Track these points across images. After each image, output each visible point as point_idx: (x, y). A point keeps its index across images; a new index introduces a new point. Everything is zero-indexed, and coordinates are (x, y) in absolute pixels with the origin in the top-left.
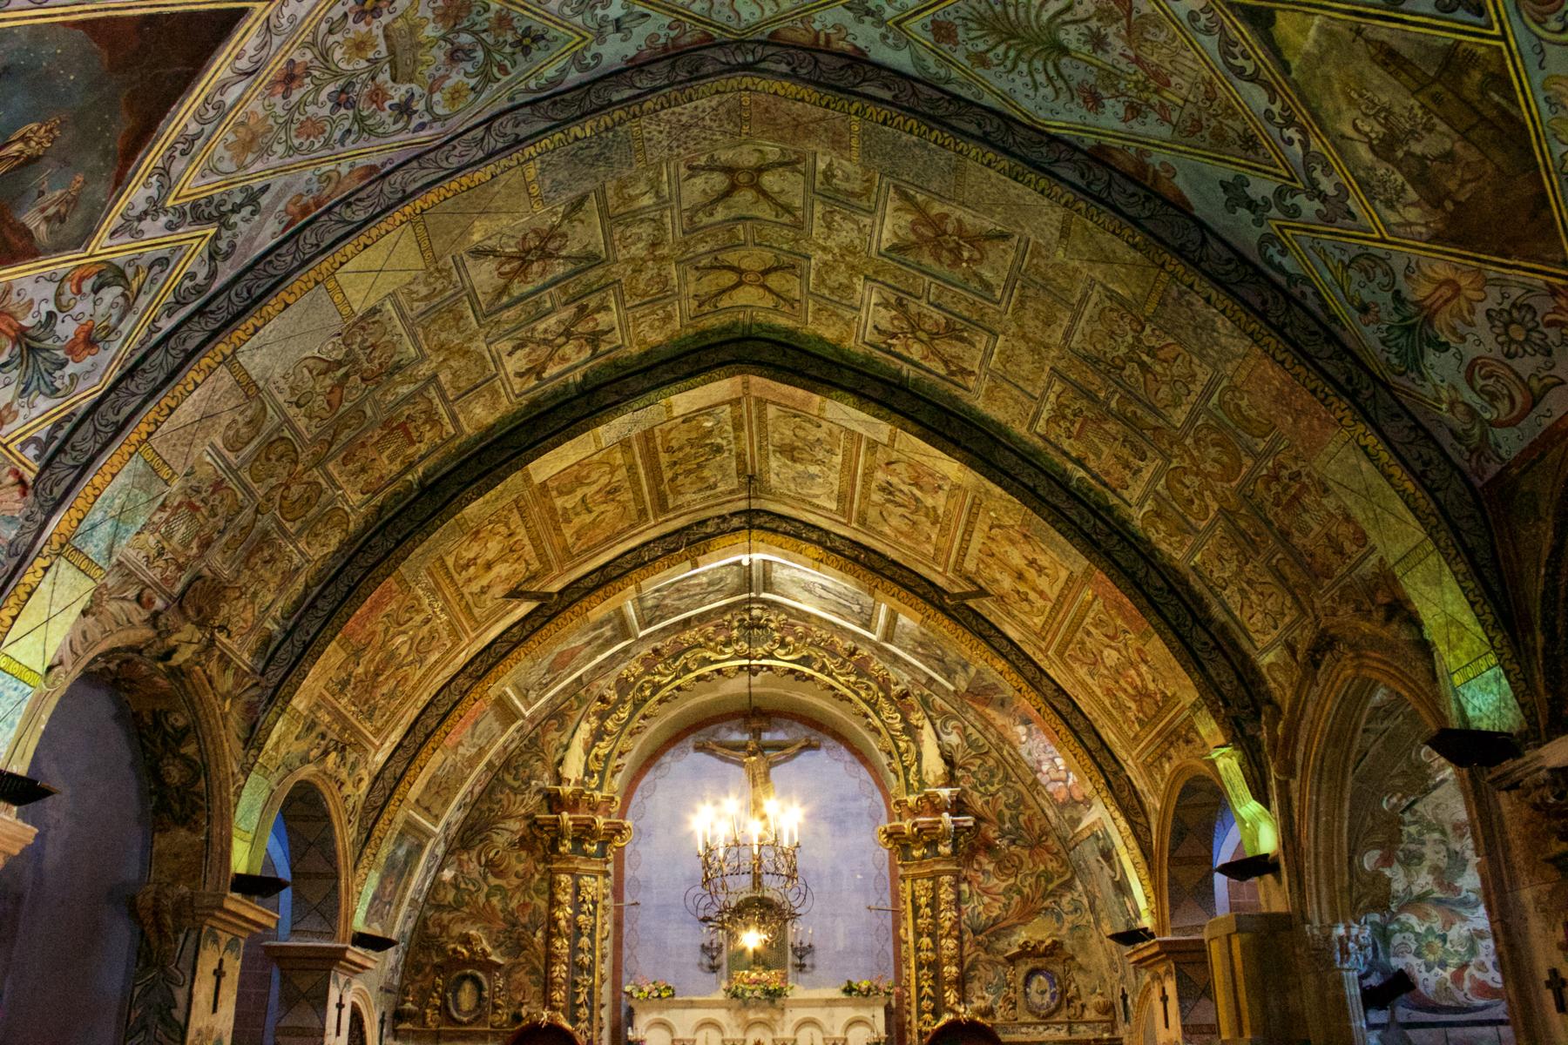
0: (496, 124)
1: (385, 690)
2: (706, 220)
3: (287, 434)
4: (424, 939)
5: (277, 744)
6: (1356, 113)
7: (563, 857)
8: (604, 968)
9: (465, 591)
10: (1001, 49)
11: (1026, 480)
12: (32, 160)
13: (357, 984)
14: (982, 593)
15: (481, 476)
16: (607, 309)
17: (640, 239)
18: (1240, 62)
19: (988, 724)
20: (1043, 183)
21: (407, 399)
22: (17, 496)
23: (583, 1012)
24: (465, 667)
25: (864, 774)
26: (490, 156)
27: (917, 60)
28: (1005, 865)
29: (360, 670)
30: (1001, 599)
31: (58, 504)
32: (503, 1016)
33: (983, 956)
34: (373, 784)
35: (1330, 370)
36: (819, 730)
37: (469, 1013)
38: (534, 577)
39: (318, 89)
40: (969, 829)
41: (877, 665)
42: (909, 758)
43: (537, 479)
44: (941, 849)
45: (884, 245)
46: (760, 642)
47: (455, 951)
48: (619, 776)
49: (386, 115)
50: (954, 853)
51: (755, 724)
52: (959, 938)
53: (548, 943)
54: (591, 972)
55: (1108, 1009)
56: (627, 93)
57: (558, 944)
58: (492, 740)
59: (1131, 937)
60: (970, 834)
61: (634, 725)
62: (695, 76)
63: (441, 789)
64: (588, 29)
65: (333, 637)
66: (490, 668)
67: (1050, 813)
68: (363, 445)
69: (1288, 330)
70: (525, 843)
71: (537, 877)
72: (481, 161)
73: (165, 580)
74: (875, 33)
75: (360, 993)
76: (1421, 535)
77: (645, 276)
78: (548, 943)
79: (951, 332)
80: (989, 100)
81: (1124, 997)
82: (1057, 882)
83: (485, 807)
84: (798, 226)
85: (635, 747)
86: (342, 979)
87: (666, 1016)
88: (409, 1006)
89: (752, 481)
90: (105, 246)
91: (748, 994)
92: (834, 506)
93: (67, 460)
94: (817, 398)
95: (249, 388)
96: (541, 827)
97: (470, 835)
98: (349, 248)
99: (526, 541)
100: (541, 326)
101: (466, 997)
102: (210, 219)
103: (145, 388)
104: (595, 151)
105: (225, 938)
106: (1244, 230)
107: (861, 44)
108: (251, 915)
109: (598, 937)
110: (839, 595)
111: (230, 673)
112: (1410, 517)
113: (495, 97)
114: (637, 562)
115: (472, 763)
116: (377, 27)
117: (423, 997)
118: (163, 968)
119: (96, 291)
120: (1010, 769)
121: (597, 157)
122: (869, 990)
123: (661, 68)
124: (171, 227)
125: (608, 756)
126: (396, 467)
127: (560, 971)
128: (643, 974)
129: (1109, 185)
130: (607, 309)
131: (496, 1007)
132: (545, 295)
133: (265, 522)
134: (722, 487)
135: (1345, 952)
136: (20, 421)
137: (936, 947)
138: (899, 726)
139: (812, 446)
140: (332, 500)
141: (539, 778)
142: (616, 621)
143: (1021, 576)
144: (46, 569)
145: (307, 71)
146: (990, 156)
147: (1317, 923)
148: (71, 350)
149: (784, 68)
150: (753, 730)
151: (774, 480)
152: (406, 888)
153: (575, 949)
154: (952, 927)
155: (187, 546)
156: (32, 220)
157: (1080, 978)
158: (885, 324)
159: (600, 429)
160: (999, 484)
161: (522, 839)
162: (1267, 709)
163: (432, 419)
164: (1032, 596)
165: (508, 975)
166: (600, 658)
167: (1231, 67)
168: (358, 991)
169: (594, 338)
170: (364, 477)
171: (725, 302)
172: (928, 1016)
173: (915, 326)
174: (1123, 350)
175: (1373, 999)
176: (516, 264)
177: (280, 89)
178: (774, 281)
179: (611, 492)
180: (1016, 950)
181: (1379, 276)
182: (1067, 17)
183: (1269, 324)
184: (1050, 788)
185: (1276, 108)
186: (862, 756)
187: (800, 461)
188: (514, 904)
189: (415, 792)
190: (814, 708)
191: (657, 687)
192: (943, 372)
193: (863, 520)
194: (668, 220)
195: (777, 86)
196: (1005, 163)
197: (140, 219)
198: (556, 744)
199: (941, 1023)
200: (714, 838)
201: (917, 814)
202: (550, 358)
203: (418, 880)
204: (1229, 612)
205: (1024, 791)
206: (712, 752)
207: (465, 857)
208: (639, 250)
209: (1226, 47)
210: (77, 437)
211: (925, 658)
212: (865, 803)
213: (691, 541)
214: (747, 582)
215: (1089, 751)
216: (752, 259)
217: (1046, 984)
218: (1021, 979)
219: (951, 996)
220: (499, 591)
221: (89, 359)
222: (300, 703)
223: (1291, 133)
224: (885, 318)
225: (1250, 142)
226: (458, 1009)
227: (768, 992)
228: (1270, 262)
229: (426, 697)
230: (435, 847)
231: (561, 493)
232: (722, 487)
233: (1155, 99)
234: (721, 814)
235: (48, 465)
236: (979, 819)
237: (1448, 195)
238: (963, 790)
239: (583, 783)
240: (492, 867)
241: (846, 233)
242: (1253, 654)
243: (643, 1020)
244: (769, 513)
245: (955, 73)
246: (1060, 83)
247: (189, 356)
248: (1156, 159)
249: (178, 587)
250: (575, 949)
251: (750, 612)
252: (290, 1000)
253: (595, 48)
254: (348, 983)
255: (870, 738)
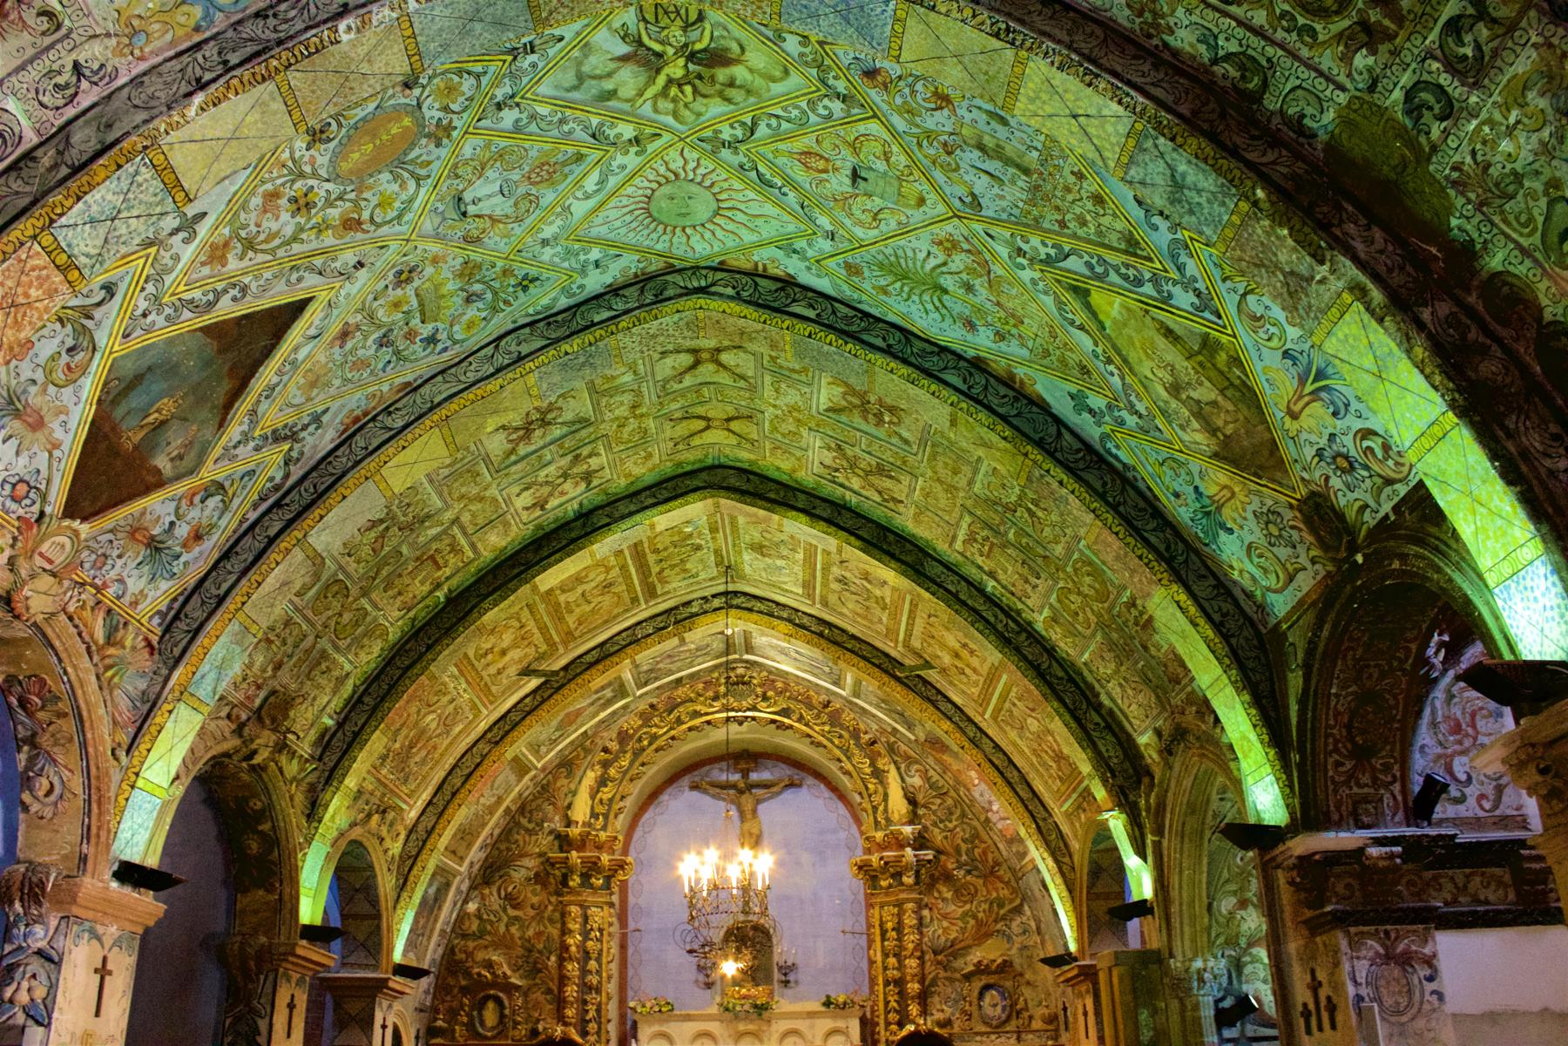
0: (503, 343)
1: (417, 759)
2: (676, 386)
3: (341, 577)
4: (451, 964)
5: (333, 817)
6: (1151, 364)
7: (572, 891)
8: (612, 987)
9: (484, 674)
10: (898, 285)
11: (950, 587)
12: (163, 423)
13: (397, 1006)
14: (928, 665)
15: (495, 591)
16: (598, 455)
17: (622, 404)
18: (1070, 316)
19: (946, 769)
20: (933, 387)
21: (436, 538)
22: (147, 656)
23: (592, 1027)
24: (485, 733)
25: (842, 809)
26: (498, 371)
27: (835, 285)
28: (962, 893)
29: (397, 745)
30: (944, 671)
31: (178, 661)
32: (522, 1031)
33: (942, 974)
34: (408, 837)
35: (1153, 540)
36: (801, 770)
37: (493, 1028)
38: (541, 657)
39: (366, 338)
40: (929, 861)
41: (848, 717)
42: (877, 799)
43: (543, 588)
44: (905, 879)
45: (822, 407)
46: (742, 696)
47: (479, 974)
48: (621, 817)
49: (418, 346)
50: (917, 883)
51: (743, 765)
52: (921, 958)
53: (561, 966)
54: (598, 991)
55: (1051, 1019)
56: (606, 314)
57: (570, 967)
58: (508, 791)
59: (1060, 960)
60: (929, 867)
61: (634, 771)
62: (660, 300)
63: (466, 835)
64: (573, 270)
65: (377, 727)
66: (507, 733)
67: (1001, 846)
68: (400, 575)
69: (1121, 509)
70: (540, 879)
71: (550, 908)
72: (492, 375)
73: (248, 698)
74: (803, 265)
75: (399, 1015)
76: (1219, 671)
77: (627, 429)
78: (561, 966)
79: (881, 470)
80: (891, 318)
81: (1065, 1009)
82: (1008, 907)
83: (503, 846)
84: (752, 389)
85: (636, 790)
86: (385, 1004)
87: (664, 1028)
88: (440, 1023)
89: (728, 570)
90: (210, 472)
91: (738, 1008)
92: (800, 591)
93: (182, 625)
94: (776, 517)
95: (317, 560)
96: (553, 865)
97: (491, 871)
98: (391, 451)
99: (535, 631)
100: (542, 473)
101: (490, 1015)
102: (286, 438)
103: (238, 568)
104: (582, 359)
105: (295, 976)
106: (1091, 430)
107: (791, 271)
108: (315, 958)
109: (604, 960)
110: (811, 659)
111: (295, 762)
112: (1211, 656)
113: (501, 323)
114: (631, 639)
115: (491, 811)
116: (409, 290)
117: (452, 1014)
118: (248, 1004)
119: (202, 502)
120: (965, 809)
121: (583, 365)
122: (845, 1003)
123: (632, 292)
124: (257, 449)
125: (611, 800)
126: (426, 588)
127: (571, 991)
128: (647, 987)
129: (986, 388)
130: (598, 455)
131: (516, 1023)
132: (546, 451)
133: (324, 643)
134: (703, 576)
135: (1201, 980)
136: (149, 599)
137: (901, 966)
138: (868, 770)
139: (777, 545)
140: (375, 619)
141: (551, 820)
142: (616, 686)
143: (957, 655)
144: (170, 712)
145: (358, 328)
146: (892, 365)
147: (1180, 958)
148: (184, 545)
149: (730, 291)
150: (742, 771)
151: (748, 570)
152: (436, 921)
153: (584, 972)
154: (915, 949)
155: (264, 671)
156: (162, 462)
157: (1027, 992)
158: (828, 462)
159: (595, 547)
160: (927, 590)
161: (537, 875)
162: (1146, 780)
163: (455, 549)
164: (967, 671)
165: (526, 995)
166: (602, 715)
167: (1066, 319)
168: (397, 1014)
169: (587, 477)
170: (400, 598)
171: (696, 441)
172: (894, 1027)
173: (853, 465)
174: (1014, 498)
175: (1224, 1018)
176: (521, 433)
177: (338, 343)
178: (734, 425)
179: (607, 586)
180: (971, 968)
181: (1183, 476)
182: (944, 269)
183: (1107, 503)
184: (1000, 826)
185: (1100, 350)
186: (842, 796)
187: (769, 556)
188: (530, 933)
189: (443, 842)
190: (793, 750)
191: (654, 737)
192: (878, 499)
193: (825, 603)
194: (644, 389)
195: (725, 306)
196: (905, 370)
197: (235, 447)
198: (565, 790)
199: (904, 1033)
200: (698, 881)
201: (885, 849)
202: (551, 494)
203: (447, 913)
204: (1112, 699)
205: (980, 828)
206: (705, 792)
207: (486, 891)
208: (622, 411)
209: (1060, 305)
210: (188, 608)
211: (889, 712)
212: (842, 835)
213: (678, 618)
214: (729, 646)
215: (1022, 800)
216: (717, 411)
217: (998, 998)
218: (976, 994)
219: (914, 1009)
220: (513, 671)
221: (197, 549)
222: (351, 782)
223: (1111, 368)
224: (828, 457)
225: (1085, 370)
226: (482, 1023)
227: (756, 1006)
228: (1110, 454)
229: (452, 761)
230: (460, 884)
231: (563, 591)
232: (703, 576)
233: (1014, 331)
234: (706, 859)
235: (167, 630)
236: (939, 852)
237: (1218, 429)
238: (925, 828)
239: (590, 825)
240: (512, 900)
241: (791, 397)
242: (1135, 735)
243: (645, 1032)
244: (745, 594)
245: (864, 297)
246: (944, 311)
247: (272, 541)
248: (1020, 372)
249: (258, 702)
250: (584, 972)
251: (736, 677)
252: (342, 1024)
253: (579, 281)
254: (390, 1006)
255: (845, 779)
